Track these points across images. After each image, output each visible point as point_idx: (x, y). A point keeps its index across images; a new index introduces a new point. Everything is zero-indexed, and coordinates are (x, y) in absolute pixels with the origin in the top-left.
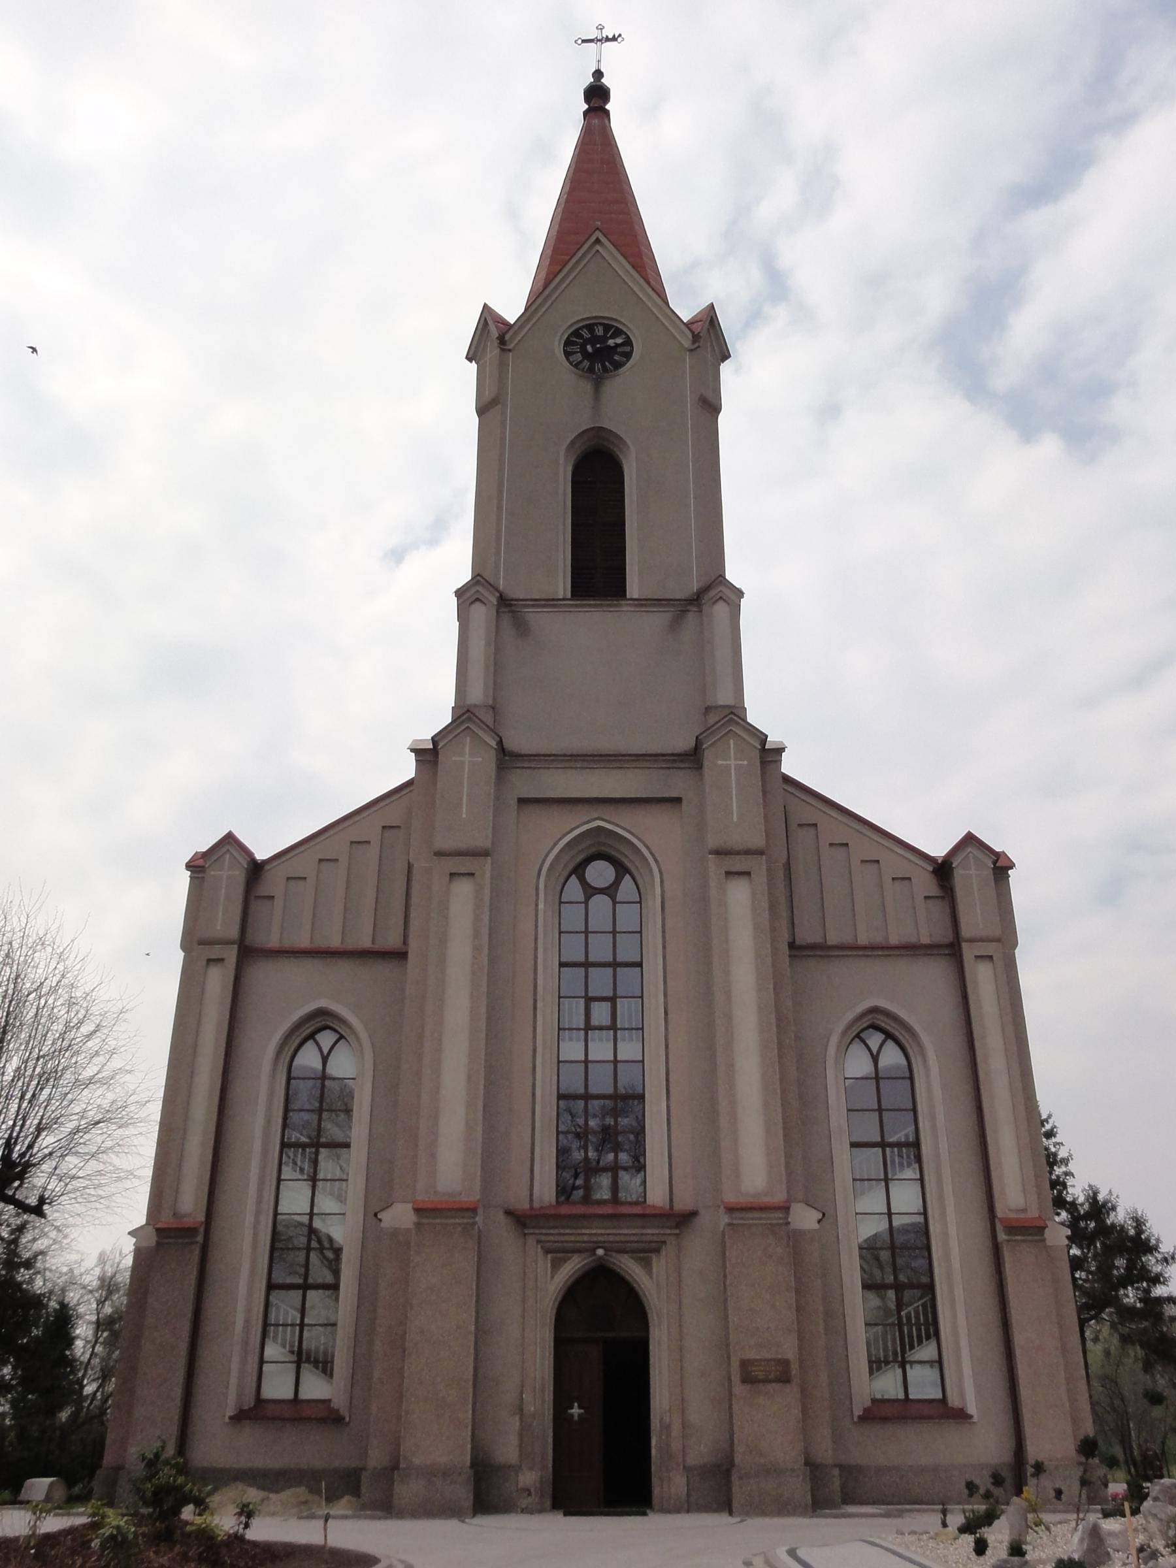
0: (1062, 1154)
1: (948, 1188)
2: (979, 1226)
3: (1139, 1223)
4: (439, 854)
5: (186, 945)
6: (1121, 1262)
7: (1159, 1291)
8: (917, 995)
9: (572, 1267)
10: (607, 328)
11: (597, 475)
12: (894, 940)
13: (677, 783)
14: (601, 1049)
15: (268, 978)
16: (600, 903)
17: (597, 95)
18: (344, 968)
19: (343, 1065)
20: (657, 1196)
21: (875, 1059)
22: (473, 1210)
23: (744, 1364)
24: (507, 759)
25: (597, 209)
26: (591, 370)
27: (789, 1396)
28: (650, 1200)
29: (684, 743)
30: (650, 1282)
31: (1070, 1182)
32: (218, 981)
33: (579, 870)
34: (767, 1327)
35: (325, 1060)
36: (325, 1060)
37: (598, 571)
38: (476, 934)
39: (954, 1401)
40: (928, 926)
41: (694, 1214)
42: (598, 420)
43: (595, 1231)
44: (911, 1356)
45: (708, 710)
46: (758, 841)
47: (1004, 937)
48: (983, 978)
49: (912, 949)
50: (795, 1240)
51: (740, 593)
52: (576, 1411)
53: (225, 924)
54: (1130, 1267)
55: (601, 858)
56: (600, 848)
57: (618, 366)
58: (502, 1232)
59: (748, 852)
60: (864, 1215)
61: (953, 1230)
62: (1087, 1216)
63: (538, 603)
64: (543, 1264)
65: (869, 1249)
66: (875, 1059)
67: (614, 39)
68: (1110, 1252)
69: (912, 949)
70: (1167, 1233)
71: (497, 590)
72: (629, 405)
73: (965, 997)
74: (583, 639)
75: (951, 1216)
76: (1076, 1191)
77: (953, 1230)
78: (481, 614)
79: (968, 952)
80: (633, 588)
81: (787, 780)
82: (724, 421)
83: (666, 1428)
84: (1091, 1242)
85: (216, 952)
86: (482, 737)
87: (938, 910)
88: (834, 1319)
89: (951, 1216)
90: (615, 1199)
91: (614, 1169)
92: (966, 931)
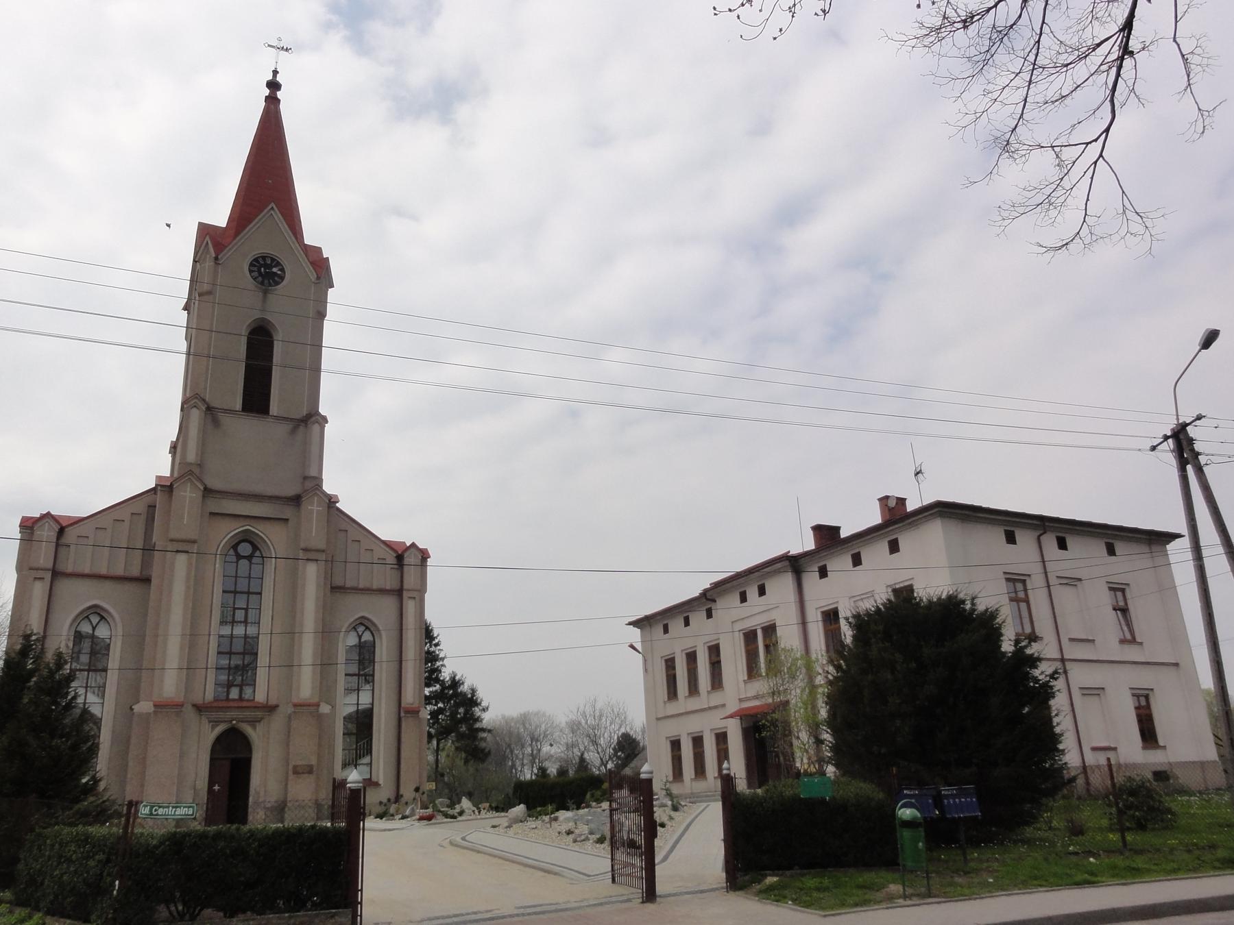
0: (441, 655)
1: (383, 695)
2: (394, 709)
3: (473, 691)
4: (172, 540)
5: (20, 568)
6: (461, 710)
7: (478, 725)
8: (381, 612)
9: (221, 728)
10: (273, 260)
11: (260, 341)
12: (375, 587)
13: (287, 512)
14: (239, 630)
15: (66, 588)
16: (244, 562)
17: (274, 85)
18: (108, 586)
19: (102, 632)
20: (260, 697)
21: (360, 637)
22: (182, 705)
23: (295, 767)
24: (208, 492)
25: (268, 175)
26: (262, 283)
27: (312, 777)
28: (257, 699)
29: (291, 491)
30: (255, 735)
31: (443, 669)
32: (39, 591)
33: (235, 547)
34: (304, 750)
35: (94, 629)
36: (94, 629)
37: (256, 399)
38: (188, 579)
39: (374, 779)
40: (390, 582)
41: (277, 706)
42: (258, 291)
43: (234, 714)
44: (360, 762)
45: (305, 478)
46: (322, 546)
47: (422, 589)
48: (410, 607)
49: (382, 591)
50: (319, 717)
51: (325, 420)
52: (216, 788)
53: (44, 557)
54: (465, 714)
55: (247, 548)
56: (247, 538)
57: (277, 283)
58: (189, 712)
59: (318, 551)
60: (347, 705)
61: (383, 712)
62: (450, 687)
63: (226, 411)
64: (206, 726)
65: (348, 719)
66: (360, 637)
67: (287, 50)
68: (457, 705)
69: (382, 591)
70: (483, 695)
71: (204, 400)
72: (280, 308)
73: (401, 614)
74: (246, 429)
75: (383, 705)
76: (446, 675)
77: (383, 712)
78: (196, 415)
79: (405, 594)
80: (274, 409)
81: (338, 509)
82: (327, 324)
83: (258, 793)
84: (449, 701)
85: (40, 574)
86: (190, 469)
87: (396, 574)
88: (332, 747)
89: (383, 705)
90: (241, 699)
91: (241, 686)
92: (405, 587)
